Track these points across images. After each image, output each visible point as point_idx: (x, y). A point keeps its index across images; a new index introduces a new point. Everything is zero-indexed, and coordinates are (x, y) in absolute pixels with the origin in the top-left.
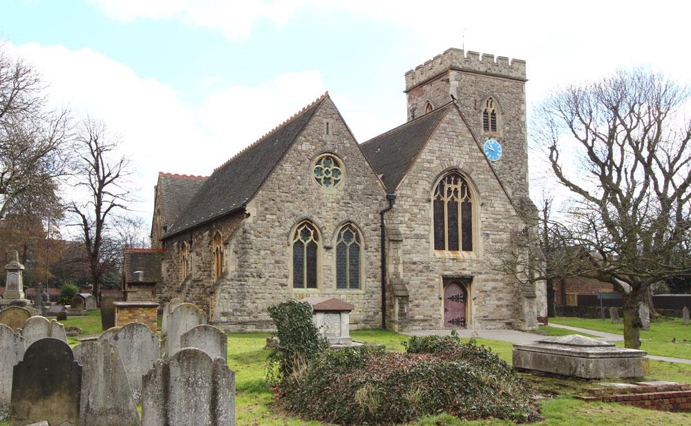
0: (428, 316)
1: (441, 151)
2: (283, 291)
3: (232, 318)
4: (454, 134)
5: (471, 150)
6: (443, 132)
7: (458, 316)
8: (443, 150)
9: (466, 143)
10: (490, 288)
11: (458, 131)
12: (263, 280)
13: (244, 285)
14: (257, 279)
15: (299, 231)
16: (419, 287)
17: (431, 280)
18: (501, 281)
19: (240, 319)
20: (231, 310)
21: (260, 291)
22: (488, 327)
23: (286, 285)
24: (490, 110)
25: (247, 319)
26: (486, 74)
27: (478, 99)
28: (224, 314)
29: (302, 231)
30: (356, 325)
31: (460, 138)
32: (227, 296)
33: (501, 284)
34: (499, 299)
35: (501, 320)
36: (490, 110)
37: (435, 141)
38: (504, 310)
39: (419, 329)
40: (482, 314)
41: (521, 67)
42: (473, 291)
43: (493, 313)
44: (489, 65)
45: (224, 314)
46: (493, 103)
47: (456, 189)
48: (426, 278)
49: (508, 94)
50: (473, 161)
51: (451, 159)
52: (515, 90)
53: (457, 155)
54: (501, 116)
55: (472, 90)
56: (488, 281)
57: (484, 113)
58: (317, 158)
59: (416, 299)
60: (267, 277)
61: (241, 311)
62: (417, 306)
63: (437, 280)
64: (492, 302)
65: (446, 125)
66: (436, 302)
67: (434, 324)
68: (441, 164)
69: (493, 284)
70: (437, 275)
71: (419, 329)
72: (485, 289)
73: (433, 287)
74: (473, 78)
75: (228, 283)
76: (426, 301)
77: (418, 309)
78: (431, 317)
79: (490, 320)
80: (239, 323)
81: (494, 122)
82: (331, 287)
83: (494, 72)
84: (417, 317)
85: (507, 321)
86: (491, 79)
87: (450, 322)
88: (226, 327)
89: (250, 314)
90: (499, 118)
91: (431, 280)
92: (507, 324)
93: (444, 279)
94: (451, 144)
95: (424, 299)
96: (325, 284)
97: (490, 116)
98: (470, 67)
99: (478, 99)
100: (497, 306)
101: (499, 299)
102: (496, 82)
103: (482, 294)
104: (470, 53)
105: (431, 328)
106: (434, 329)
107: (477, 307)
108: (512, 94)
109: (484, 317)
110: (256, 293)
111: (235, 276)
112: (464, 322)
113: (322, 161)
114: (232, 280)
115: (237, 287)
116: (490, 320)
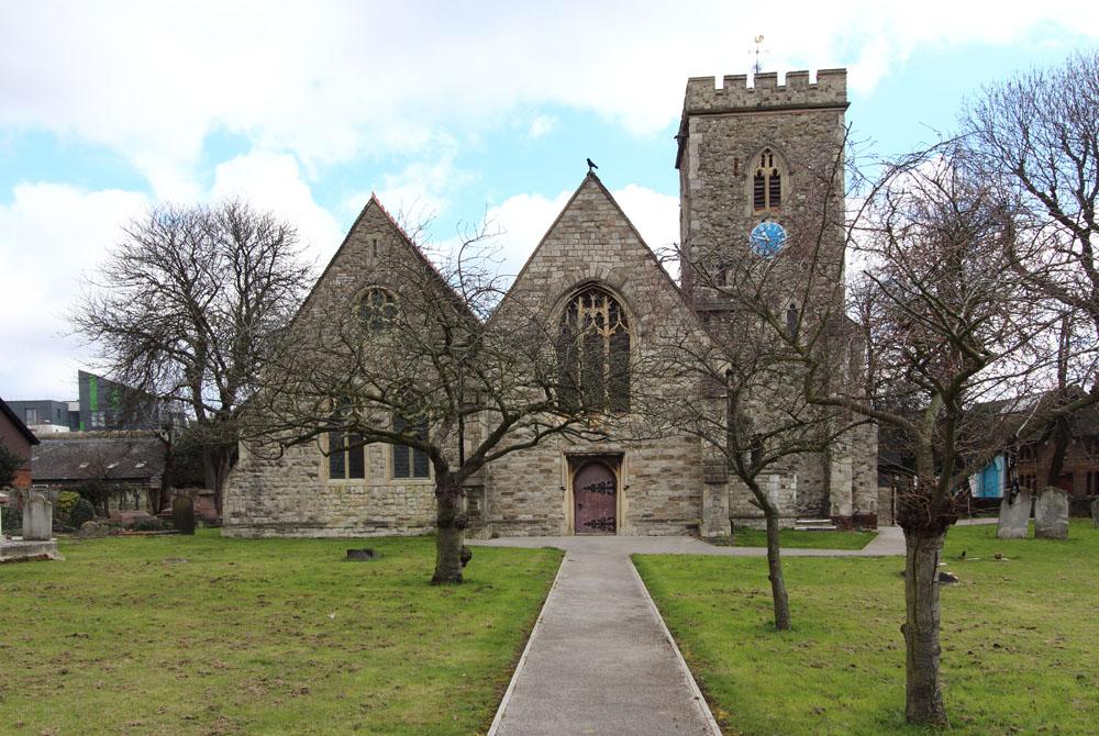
0: (540, 516)
1: (566, 256)
2: (312, 483)
3: (245, 519)
4: (593, 224)
5: (625, 247)
6: (571, 224)
7: (604, 514)
8: (571, 253)
9: (615, 235)
10: (657, 470)
11: (601, 218)
12: (285, 469)
13: (259, 476)
14: (276, 468)
16: (526, 472)
17: (547, 460)
18: (679, 458)
19: (256, 520)
20: (243, 510)
21: (282, 484)
22: (650, 532)
23: (316, 475)
24: (767, 171)
25: (266, 520)
26: (759, 109)
27: (742, 156)
28: (235, 515)
30: (420, 529)
31: (604, 230)
32: (238, 491)
33: (681, 463)
34: (675, 488)
35: (676, 520)
36: (767, 171)
37: (555, 242)
38: (684, 504)
39: (524, 535)
40: (641, 511)
41: (835, 82)
42: (625, 476)
43: (663, 510)
44: (766, 93)
45: (235, 515)
46: (774, 158)
47: (599, 314)
48: (536, 458)
49: (806, 137)
50: (628, 264)
51: (586, 267)
52: (821, 128)
53: (599, 258)
54: (787, 177)
55: (729, 143)
56: (654, 458)
57: (756, 179)
58: (361, 294)
59: (520, 490)
60: (290, 465)
61: (256, 510)
62: (522, 500)
63: (557, 460)
64: (661, 493)
65: (577, 212)
66: (555, 494)
67: (550, 527)
68: (566, 276)
69: (664, 464)
70: (558, 453)
71: (524, 535)
72: (646, 471)
73: (550, 471)
74: (733, 122)
75: (239, 474)
76: (537, 494)
77: (521, 505)
78: (546, 516)
79: (655, 521)
80: (254, 526)
81: (776, 192)
82: (382, 475)
83: (775, 103)
84: (521, 517)
85: (688, 523)
86: (771, 117)
87: (589, 524)
88: (236, 530)
89: (268, 514)
90: (785, 182)
91: (547, 460)
92: (689, 527)
93: (568, 458)
94: (586, 241)
95: (533, 490)
96: (372, 471)
97: (767, 181)
98: (725, 103)
99: (742, 156)
100: (670, 499)
101: (675, 488)
102: (781, 119)
103: (641, 480)
104: (727, 79)
105: (546, 533)
106: (549, 534)
107: (632, 500)
108: (814, 136)
109: (644, 516)
110: (276, 487)
111: (247, 466)
112: (614, 524)
113: (370, 297)
114: (243, 470)
115: (251, 480)
116: (655, 521)
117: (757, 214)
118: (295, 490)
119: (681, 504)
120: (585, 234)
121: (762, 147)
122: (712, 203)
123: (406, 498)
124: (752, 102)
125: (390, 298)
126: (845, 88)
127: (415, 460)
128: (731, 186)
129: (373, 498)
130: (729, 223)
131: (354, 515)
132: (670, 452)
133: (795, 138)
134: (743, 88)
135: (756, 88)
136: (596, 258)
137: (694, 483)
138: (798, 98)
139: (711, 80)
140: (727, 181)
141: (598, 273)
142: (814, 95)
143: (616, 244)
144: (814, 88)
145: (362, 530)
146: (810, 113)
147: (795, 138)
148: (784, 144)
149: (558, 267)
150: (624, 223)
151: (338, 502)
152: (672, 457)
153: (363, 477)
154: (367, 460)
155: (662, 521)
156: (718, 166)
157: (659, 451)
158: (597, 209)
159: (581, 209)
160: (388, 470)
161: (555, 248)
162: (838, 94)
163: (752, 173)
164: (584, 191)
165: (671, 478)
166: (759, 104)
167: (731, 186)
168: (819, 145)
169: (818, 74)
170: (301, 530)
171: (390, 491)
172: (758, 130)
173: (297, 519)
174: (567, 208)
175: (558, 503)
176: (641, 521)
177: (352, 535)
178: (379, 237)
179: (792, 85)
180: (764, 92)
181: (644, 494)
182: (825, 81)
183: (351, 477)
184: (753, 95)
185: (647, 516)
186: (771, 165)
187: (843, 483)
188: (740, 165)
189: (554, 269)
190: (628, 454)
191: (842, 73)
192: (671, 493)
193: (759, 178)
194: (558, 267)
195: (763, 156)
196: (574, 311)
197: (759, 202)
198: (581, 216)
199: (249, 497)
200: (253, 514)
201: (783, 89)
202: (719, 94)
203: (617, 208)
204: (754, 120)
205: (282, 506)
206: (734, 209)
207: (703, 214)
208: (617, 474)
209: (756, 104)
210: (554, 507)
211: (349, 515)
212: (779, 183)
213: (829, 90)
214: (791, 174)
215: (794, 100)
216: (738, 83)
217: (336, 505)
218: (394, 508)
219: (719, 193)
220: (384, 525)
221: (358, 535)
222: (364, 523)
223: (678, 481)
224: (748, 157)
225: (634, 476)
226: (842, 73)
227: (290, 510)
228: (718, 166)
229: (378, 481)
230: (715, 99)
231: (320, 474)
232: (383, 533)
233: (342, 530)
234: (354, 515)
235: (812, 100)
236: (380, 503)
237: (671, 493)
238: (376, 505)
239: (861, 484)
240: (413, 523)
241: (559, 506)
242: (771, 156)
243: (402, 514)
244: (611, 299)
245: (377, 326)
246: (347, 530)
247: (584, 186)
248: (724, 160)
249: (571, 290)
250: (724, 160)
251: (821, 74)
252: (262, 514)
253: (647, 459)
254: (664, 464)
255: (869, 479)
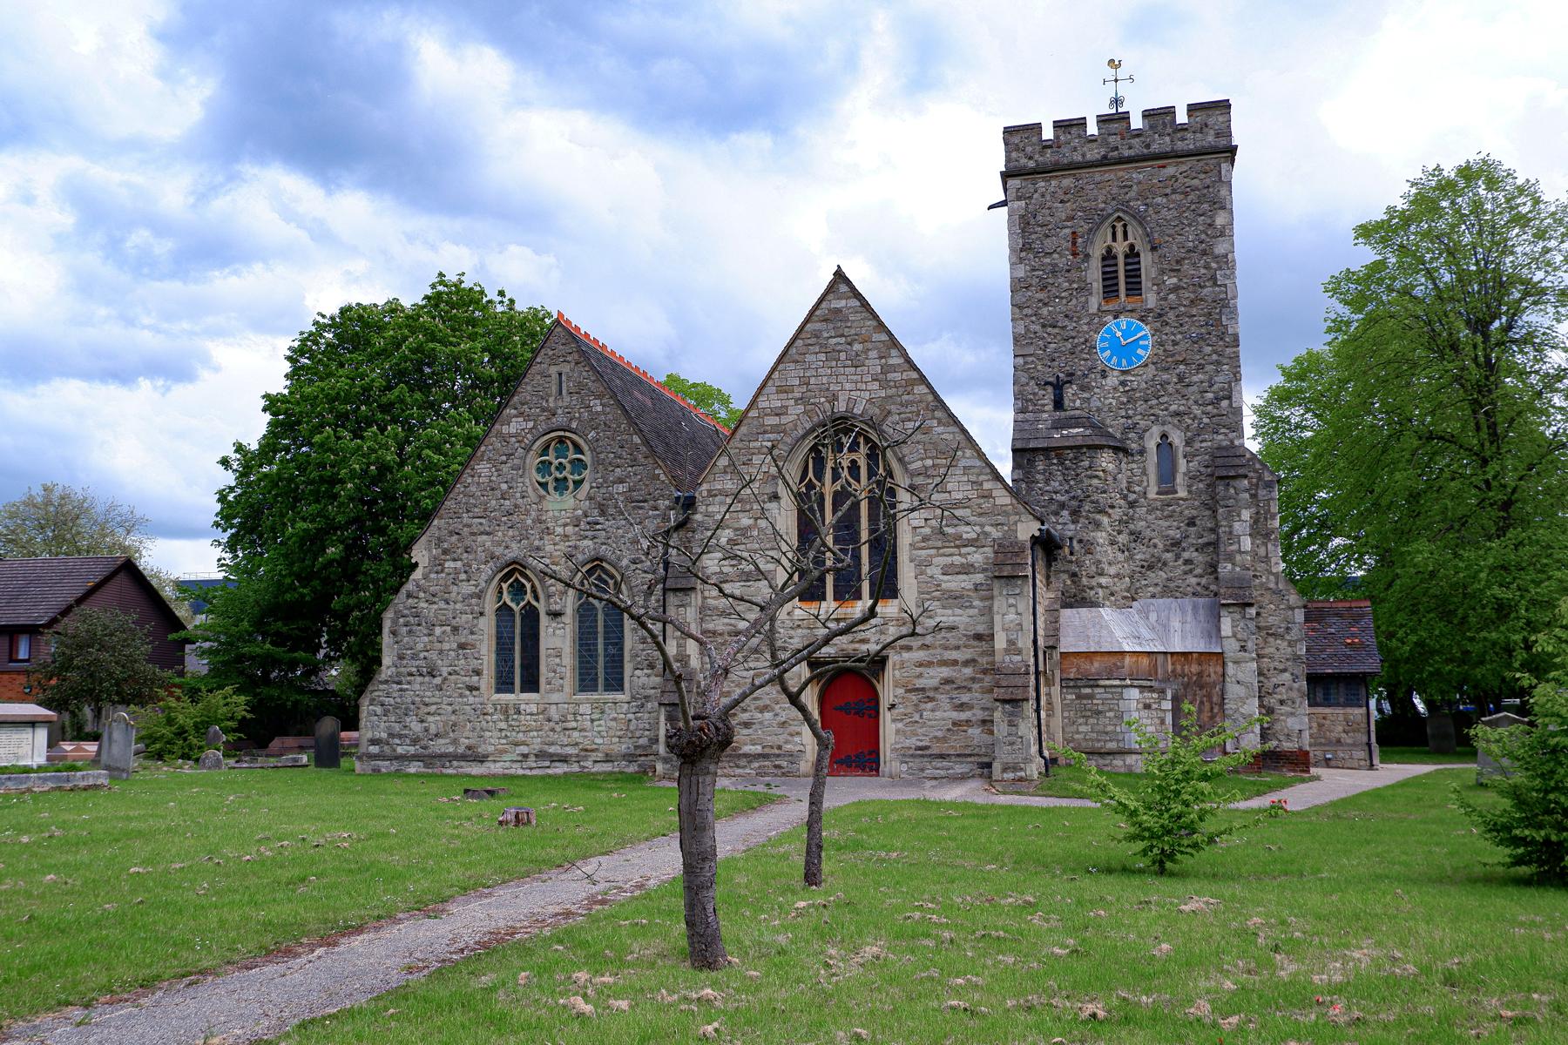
0: (772, 747)
1: (808, 384)
2: (471, 699)
4: (843, 340)
5: (886, 369)
8: (813, 381)
9: (873, 354)
10: (934, 682)
11: (853, 332)
12: (438, 680)
14: (427, 679)
15: (505, 586)
18: (967, 663)
19: (400, 750)
20: (384, 735)
21: (434, 700)
24: (1120, 248)
25: (412, 750)
26: (1104, 162)
28: (374, 742)
29: (511, 585)
32: (379, 710)
33: (968, 671)
34: (961, 707)
36: (1120, 248)
37: (792, 366)
40: (913, 742)
41: (1215, 119)
42: (888, 690)
43: (944, 739)
45: (374, 742)
46: (1129, 229)
47: (854, 462)
55: (1062, 212)
56: (930, 664)
57: (1104, 259)
60: (445, 674)
61: (400, 736)
64: (942, 714)
65: (818, 326)
69: (945, 672)
72: (920, 683)
74: (1067, 182)
75: (381, 687)
76: (768, 715)
78: (780, 747)
81: (1134, 277)
82: (561, 689)
83: (1126, 153)
86: (1121, 172)
89: (415, 741)
90: (1146, 260)
96: (550, 684)
97: (1121, 260)
100: (954, 724)
102: (1138, 175)
103: (914, 697)
104: (1058, 125)
105: (779, 772)
107: (900, 725)
108: (1186, 194)
114: (386, 682)
117: (1110, 307)
118: (450, 709)
119: (970, 731)
120: (831, 354)
121: (1111, 215)
122: (1041, 295)
123: (592, 721)
124: (1094, 154)
125: (578, 449)
126: (1229, 126)
127: (606, 668)
128: (1068, 271)
129: (549, 720)
130: (1067, 322)
131: (524, 743)
132: (954, 655)
133: (1159, 200)
134: (1079, 136)
135: (1100, 134)
136: (848, 386)
137: (987, 700)
138: (1161, 144)
139: (1037, 128)
140: (1062, 263)
141: (851, 406)
142: (1183, 139)
143: (873, 364)
144: (1183, 128)
145: (534, 765)
146: (1178, 164)
147: (1159, 200)
148: (1142, 208)
149: (796, 400)
150: (884, 337)
151: (503, 725)
152: (955, 663)
153: (537, 691)
154: (543, 668)
155: (942, 756)
156: (1049, 244)
157: (938, 654)
158: (848, 320)
159: (825, 320)
160: (569, 682)
161: (793, 375)
162: (1218, 135)
163: (1097, 251)
164: (831, 296)
165: (955, 694)
166: (1105, 157)
167: (1068, 271)
168: (1193, 207)
169: (1189, 111)
170: (455, 763)
171: (571, 710)
172: (1104, 191)
173: (451, 749)
174: (808, 319)
175: (797, 729)
176: (912, 755)
177: (521, 772)
178: (566, 368)
179: (1151, 127)
180: (1111, 139)
181: (916, 717)
182: (1200, 117)
183: (522, 691)
184: (1094, 145)
185: (920, 748)
186: (1126, 237)
187: (1243, 700)
188: (1080, 240)
189: (792, 402)
190: (893, 658)
191: (1224, 106)
192: (955, 715)
193: (1109, 256)
194: (796, 400)
195: (1114, 227)
196: (820, 463)
197: (1110, 290)
198: (827, 331)
199: (393, 719)
200: (398, 741)
201: (1138, 134)
202: (1047, 146)
203: (875, 316)
204: (1098, 178)
205: (433, 730)
206: (1074, 301)
207: (1029, 311)
208: (879, 688)
209: (1099, 157)
210: (792, 735)
211: (517, 744)
212: (1139, 263)
213: (1205, 130)
214: (1154, 249)
215: (1155, 148)
216: (1074, 130)
217: (501, 730)
218: (576, 734)
219: (1050, 281)
220: (564, 759)
221: (528, 772)
222: (536, 756)
223: (965, 698)
224: (1090, 230)
225: (902, 691)
226: (1224, 106)
227: (441, 737)
228: (1049, 244)
229: (555, 697)
230: (1042, 153)
231: (483, 687)
232: (560, 769)
233: (507, 764)
234: (524, 743)
235: (1180, 145)
236: (558, 728)
237: (955, 715)
238: (553, 730)
239: (1282, 702)
240: (600, 756)
241: (798, 734)
242: (1125, 226)
243: (587, 744)
244: (868, 440)
245: (561, 485)
246: (514, 765)
247: (831, 289)
248: (1057, 235)
249: (813, 430)
250: (1057, 235)
251: (1193, 109)
252: (408, 741)
253: (921, 665)
254: (945, 672)
255: (1294, 694)
